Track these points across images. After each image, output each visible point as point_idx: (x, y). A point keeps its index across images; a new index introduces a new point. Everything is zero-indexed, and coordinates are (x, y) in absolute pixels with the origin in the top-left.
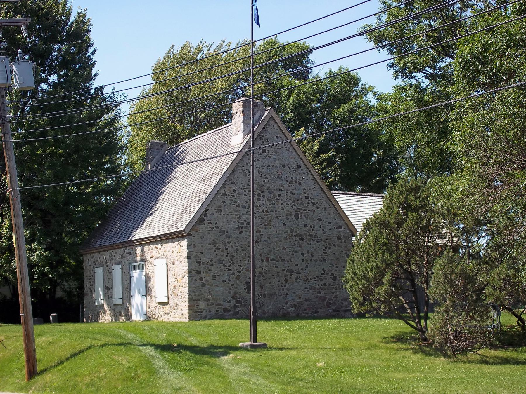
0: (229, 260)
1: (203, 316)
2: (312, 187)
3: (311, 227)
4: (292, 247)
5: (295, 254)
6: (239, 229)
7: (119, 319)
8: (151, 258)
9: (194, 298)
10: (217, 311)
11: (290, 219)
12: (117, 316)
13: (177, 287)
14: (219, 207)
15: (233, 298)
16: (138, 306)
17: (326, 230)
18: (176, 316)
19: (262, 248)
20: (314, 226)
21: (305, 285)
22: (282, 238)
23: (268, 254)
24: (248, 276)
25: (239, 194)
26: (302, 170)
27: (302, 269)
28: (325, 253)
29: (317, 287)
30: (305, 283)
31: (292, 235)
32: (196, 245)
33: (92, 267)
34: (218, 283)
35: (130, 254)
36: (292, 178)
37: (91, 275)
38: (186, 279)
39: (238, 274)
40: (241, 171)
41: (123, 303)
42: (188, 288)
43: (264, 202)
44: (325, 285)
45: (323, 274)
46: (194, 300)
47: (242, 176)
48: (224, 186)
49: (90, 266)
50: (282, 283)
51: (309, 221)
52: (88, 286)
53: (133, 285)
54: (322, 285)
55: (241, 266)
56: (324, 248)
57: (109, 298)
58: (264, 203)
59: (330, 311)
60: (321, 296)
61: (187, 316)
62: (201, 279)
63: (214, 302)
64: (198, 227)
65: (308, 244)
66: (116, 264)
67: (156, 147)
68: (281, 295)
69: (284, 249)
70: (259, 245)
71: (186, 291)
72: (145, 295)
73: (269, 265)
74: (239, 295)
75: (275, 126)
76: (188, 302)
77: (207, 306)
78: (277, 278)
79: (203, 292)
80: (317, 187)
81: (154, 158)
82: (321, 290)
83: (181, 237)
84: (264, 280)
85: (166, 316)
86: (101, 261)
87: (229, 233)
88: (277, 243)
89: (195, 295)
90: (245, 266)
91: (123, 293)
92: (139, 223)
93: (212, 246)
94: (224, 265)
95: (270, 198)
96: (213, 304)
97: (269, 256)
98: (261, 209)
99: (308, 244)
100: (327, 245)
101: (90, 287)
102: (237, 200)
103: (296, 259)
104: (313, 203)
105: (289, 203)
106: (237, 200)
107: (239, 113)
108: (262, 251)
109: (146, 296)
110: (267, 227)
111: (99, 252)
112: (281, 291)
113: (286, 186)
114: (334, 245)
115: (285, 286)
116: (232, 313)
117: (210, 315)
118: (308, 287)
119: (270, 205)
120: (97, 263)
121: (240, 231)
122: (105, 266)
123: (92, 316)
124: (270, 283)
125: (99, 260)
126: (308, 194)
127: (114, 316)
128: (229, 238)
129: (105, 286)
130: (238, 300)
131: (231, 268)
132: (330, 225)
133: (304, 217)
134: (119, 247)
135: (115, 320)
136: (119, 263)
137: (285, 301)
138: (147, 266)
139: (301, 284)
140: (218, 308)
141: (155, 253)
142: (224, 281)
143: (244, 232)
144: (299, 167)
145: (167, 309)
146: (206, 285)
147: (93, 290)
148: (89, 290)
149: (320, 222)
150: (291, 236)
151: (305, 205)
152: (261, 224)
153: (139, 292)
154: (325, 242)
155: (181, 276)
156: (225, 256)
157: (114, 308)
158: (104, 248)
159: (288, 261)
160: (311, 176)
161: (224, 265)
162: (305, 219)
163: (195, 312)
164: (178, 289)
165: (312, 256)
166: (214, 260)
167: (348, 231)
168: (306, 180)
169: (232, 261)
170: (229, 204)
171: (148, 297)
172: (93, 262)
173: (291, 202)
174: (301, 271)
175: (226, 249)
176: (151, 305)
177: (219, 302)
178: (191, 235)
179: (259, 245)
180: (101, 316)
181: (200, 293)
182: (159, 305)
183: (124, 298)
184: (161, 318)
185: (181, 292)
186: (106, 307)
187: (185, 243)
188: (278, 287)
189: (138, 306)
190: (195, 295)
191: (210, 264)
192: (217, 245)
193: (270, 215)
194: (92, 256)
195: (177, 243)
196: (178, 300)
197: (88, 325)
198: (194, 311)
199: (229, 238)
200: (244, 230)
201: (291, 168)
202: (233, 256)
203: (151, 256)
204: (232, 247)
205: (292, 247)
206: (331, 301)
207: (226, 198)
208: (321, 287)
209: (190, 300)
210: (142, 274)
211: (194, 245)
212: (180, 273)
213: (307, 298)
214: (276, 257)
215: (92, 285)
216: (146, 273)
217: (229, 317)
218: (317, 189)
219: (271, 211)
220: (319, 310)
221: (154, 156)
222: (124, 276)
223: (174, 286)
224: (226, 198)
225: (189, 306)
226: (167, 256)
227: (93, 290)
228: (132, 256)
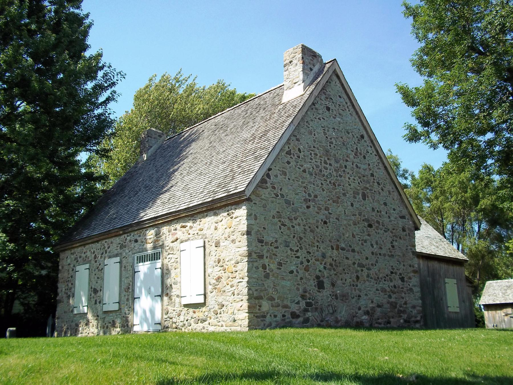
0: (296, 243)
1: (267, 323)
2: (376, 164)
3: (378, 211)
4: (361, 234)
5: (365, 244)
6: (307, 202)
7: (110, 332)
8: (173, 242)
9: (256, 294)
10: (284, 316)
11: (358, 198)
12: (107, 327)
13: (223, 280)
14: (283, 168)
15: (303, 297)
16: (145, 312)
17: (392, 219)
18: (220, 324)
19: (331, 231)
20: (380, 212)
21: (376, 285)
22: (352, 222)
23: (338, 241)
24: (318, 267)
25: (304, 156)
26: (365, 141)
27: (372, 265)
28: (393, 247)
29: (388, 289)
30: (376, 283)
31: (361, 219)
32: (258, 215)
33: (72, 266)
34: (284, 274)
35: (136, 241)
36: (357, 149)
37: (70, 276)
38: (244, 266)
39: (307, 264)
40: (306, 127)
41: (120, 309)
42: (246, 279)
43: (331, 172)
44: (395, 287)
45: (392, 273)
46: (257, 298)
47: (306, 134)
48: (288, 142)
49: (69, 264)
50: (354, 281)
51: (375, 204)
52: (64, 289)
53: (138, 284)
54: (392, 287)
55: (310, 253)
56: (391, 240)
57: (96, 303)
58: (331, 173)
59: (402, 321)
60: (392, 302)
61: (246, 322)
62: (264, 267)
63: (280, 302)
64: (259, 191)
65: (376, 232)
66: (110, 257)
67: (154, 136)
68: (354, 298)
69: (354, 236)
70: (328, 227)
71: (244, 284)
72: (160, 296)
73: (339, 256)
74: (309, 293)
75: (337, 84)
76: (248, 300)
77: (271, 308)
78: (348, 273)
79: (266, 286)
80: (381, 165)
81: (152, 147)
82: (392, 294)
83: (232, 204)
84: (336, 275)
85: (200, 324)
86: (86, 257)
87: (295, 205)
88: (347, 227)
89: (256, 290)
90: (314, 253)
91: (120, 294)
92: (145, 205)
93: (276, 220)
94: (291, 250)
95: (336, 169)
96: (278, 306)
97: (338, 243)
98: (328, 180)
99: (376, 232)
100: (394, 237)
101: (66, 291)
102: (303, 163)
103: (366, 250)
104: (378, 183)
105: (355, 178)
106: (303, 163)
107: (295, 62)
108: (331, 235)
109: (161, 296)
110: (335, 204)
111: (84, 245)
112: (353, 292)
113: (351, 157)
114: (400, 238)
115: (357, 286)
116: (301, 319)
117: (276, 321)
118: (379, 289)
119: (337, 176)
120: (79, 260)
121: (308, 205)
122: (93, 262)
123: (68, 328)
124: (342, 280)
125: (83, 255)
126: (373, 171)
127: (104, 328)
128: (296, 212)
129: (92, 288)
130: (308, 301)
131: (299, 254)
132: (394, 212)
133: (370, 198)
134: (118, 234)
135: (105, 333)
136: (116, 256)
137: (358, 305)
138: (165, 254)
139: (372, 284)
140: (285, 312)
141: (180, 234)
142: (292, 272)
143: (311, 206)
144: (362, 137)
145: (200, 313)
146: (271, 276)
147: (71, 295)
148: (65, 296)
149: (385, 207)
150: (359, 220)
151: (371, 184)
152: (329, 200)
153: (149, 292)
154: (392, 232)
155: (233, 262)
156: (292, 236)
157: (104, 316)
158: (93, 238)
159: (358, 253)
160: (374, 150)
161: (291, 250)
162: (372, 201)
163: (256, 317)
164: (225, 282)
165: (381, 248)
166: (279, 241)
167: (411, 223)
168: (370, 154)
169: (300, 244)
170: (294, 166)
171: (165, 298)
172: (74, 259)
173: (357, 177)
174: (371, 267)
175: (293, 227)
176: (170, 309)
177: (285, 302)
178: (252, 201)
179: (328, 227)
180: (80, 329)
181: (263, 288)
182: (186, 309)
183: (122, 302)
184: (190, 328)
185: (232, 286)
186: (90, 316)
187: (242, 212)
188: (351, 285)
189: (145, 312)
190: (256, 290)
191: (275, 246)
192: (282, 220)
193: (338, 190)
194: (72, 252)
195: (225, 214)
196: (227, 299)
197: (59, 339)
198: (256, 315)
199: (296, 212)
200: (311, 204)
201: (355, 137)
202: (301, 238)
203: (174, 238)
204: (299, 225)
205: (361, 234)
206: (401, 309)
207: (291, 157)
208: (391, 290)
209: (251, 297)
210: (155, 266)
211: (255, 215)
212: (231, 257)
213: (379, 304)
214: (346, 245)
215: (71, 289)
216: (163, 265)
217: (299, 325)
218: (380, 167)
219: (339, 185)
220: (392, 320)
221: (151, 145)
222: (124, 272)
223: (219, 279)
224: (291, 157)
225: (249, 307)
226: (204, 235)
227: (71, 295)
228: (139, 243)
